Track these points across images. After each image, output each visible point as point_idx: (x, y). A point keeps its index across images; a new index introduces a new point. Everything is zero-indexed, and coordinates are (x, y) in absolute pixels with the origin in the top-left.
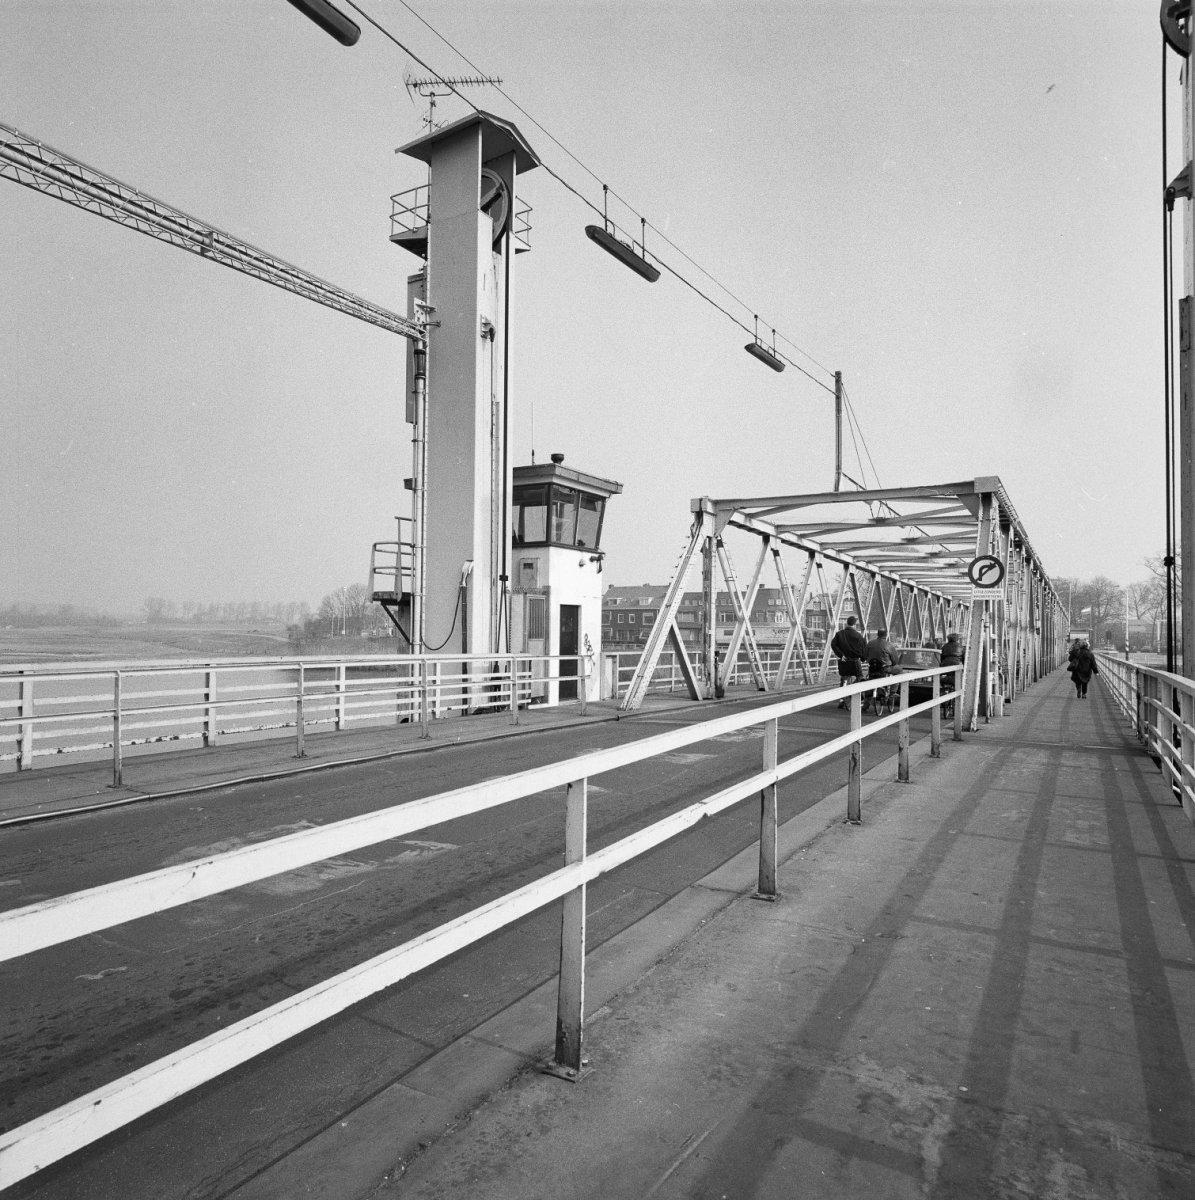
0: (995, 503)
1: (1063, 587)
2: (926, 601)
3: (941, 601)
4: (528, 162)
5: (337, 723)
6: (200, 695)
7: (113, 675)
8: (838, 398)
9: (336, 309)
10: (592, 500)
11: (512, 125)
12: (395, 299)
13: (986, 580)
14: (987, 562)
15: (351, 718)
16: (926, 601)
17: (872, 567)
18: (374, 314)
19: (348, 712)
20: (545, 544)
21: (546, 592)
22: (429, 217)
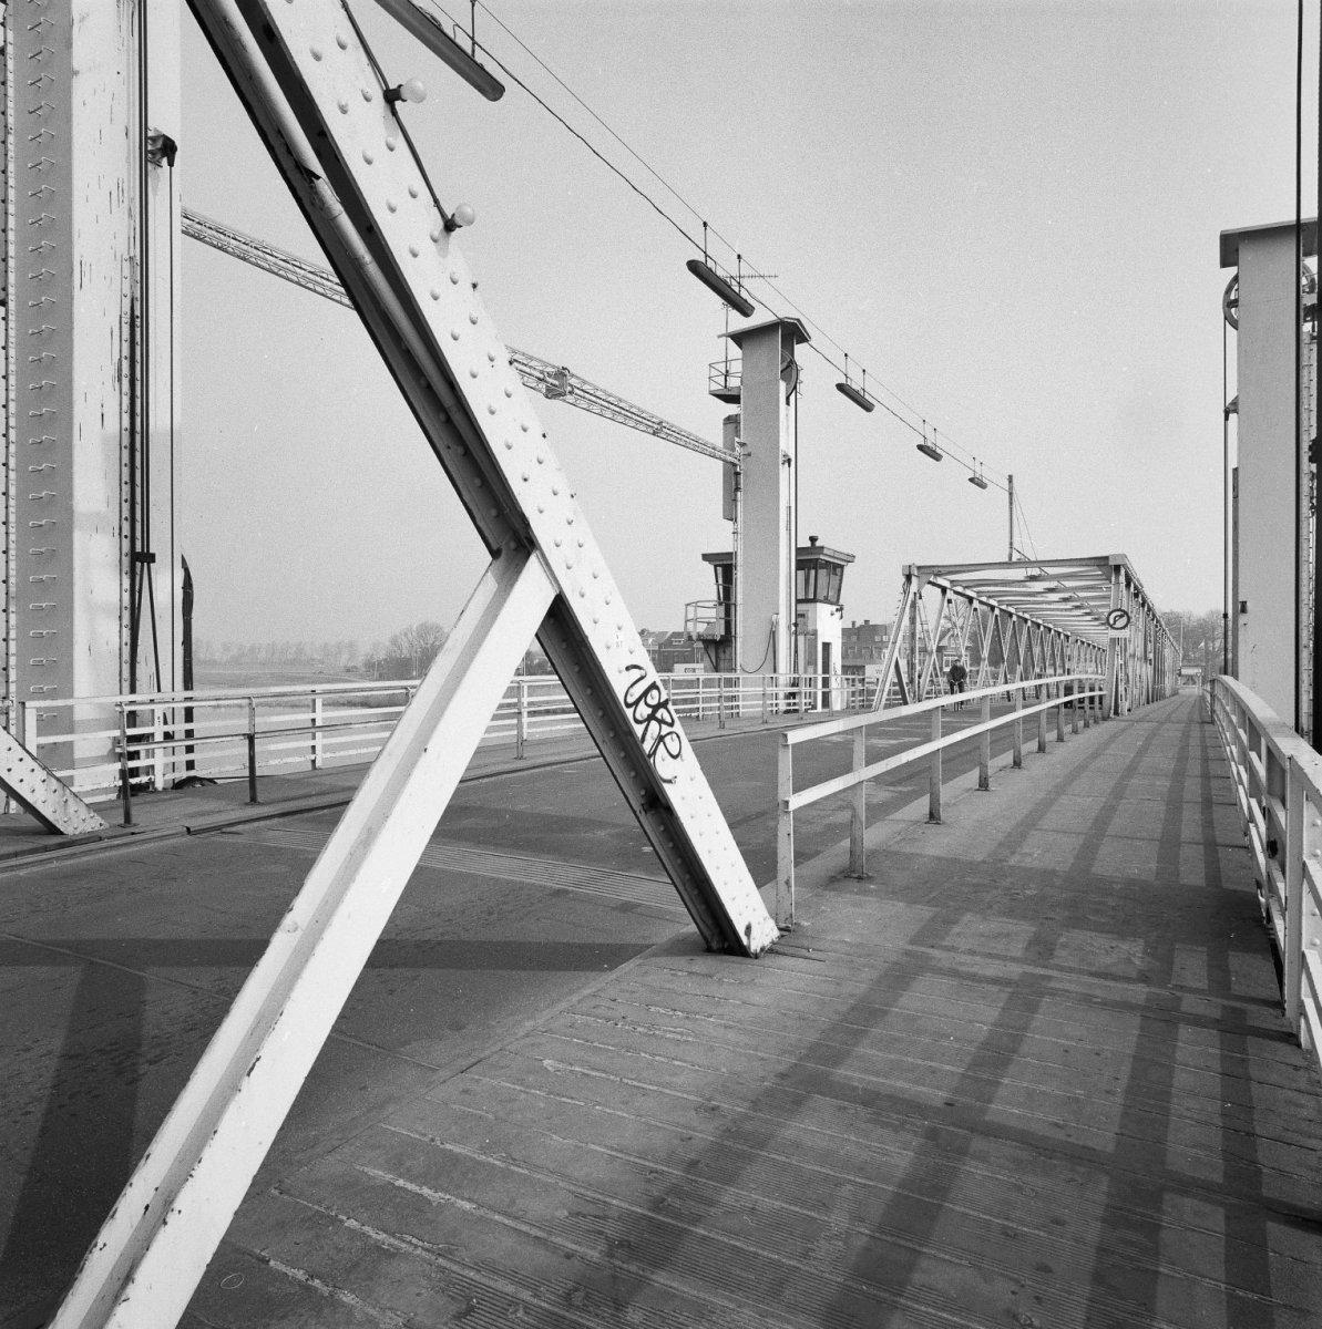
0: (1123, 571)
1: (1174, 621)
2: (1049, 637)
3: (1062, 636)
4: (803, 338)
5: (314, 762)
6: (307, 720)
7: (404, 691)
8: (1011, 494)
9: (319, 293)
10: (836, 568)
11: (798, 320)
12: (716, 436)
13: (1118, 625)
14: (1119, 613)
15: (328, 755)
16: (1049, 637)
17: (969, 593)
18: (245, 247)
19: (530, 725)
20: (814, 600)
21: (815, 633)
22: (727, 371)
